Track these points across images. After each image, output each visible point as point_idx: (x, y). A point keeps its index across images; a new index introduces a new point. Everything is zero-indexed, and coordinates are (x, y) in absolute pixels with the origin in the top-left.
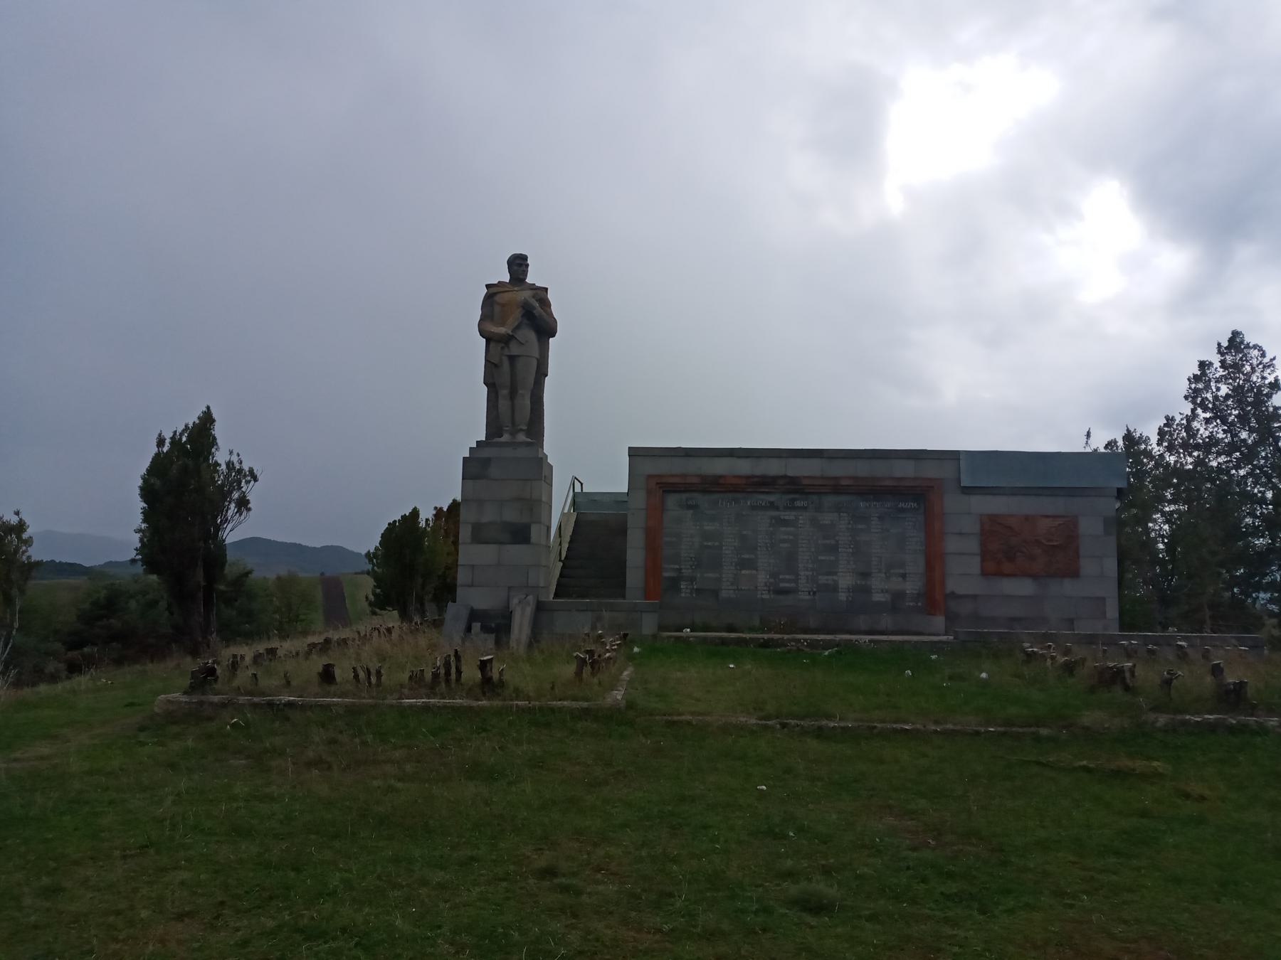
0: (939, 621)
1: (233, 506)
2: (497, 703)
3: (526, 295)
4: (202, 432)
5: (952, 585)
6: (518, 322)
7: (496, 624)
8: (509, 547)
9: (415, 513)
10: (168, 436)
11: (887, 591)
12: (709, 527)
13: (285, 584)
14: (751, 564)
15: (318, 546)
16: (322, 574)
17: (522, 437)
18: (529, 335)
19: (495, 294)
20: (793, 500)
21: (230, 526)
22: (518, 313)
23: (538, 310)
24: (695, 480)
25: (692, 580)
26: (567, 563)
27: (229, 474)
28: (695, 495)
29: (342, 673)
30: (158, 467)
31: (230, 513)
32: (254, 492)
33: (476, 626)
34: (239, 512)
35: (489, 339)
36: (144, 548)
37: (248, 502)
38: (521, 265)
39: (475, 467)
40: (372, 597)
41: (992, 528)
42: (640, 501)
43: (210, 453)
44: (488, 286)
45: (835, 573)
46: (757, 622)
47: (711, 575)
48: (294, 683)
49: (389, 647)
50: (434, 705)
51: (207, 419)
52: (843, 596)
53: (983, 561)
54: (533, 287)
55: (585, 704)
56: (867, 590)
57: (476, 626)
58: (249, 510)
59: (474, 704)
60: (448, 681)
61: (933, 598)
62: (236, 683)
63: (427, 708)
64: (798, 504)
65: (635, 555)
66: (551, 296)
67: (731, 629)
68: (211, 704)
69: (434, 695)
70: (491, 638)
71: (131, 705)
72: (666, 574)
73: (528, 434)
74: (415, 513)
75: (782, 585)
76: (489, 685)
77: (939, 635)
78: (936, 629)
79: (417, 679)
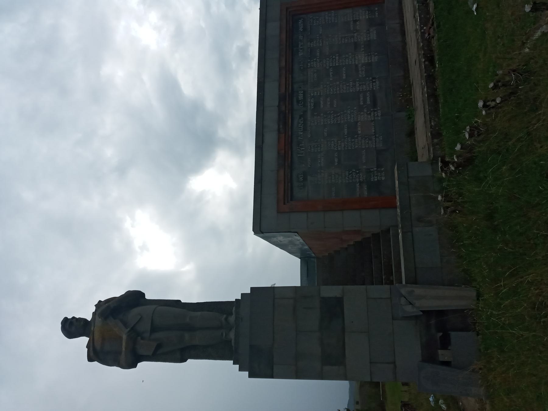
6: (130, 330)
17: (232, 319)
20: (298, 101)
24: (282, 173)
33: (443, 355)
45: (356, 66)
52: (375, 59)
65: (351, 220)
75: (368, 102)
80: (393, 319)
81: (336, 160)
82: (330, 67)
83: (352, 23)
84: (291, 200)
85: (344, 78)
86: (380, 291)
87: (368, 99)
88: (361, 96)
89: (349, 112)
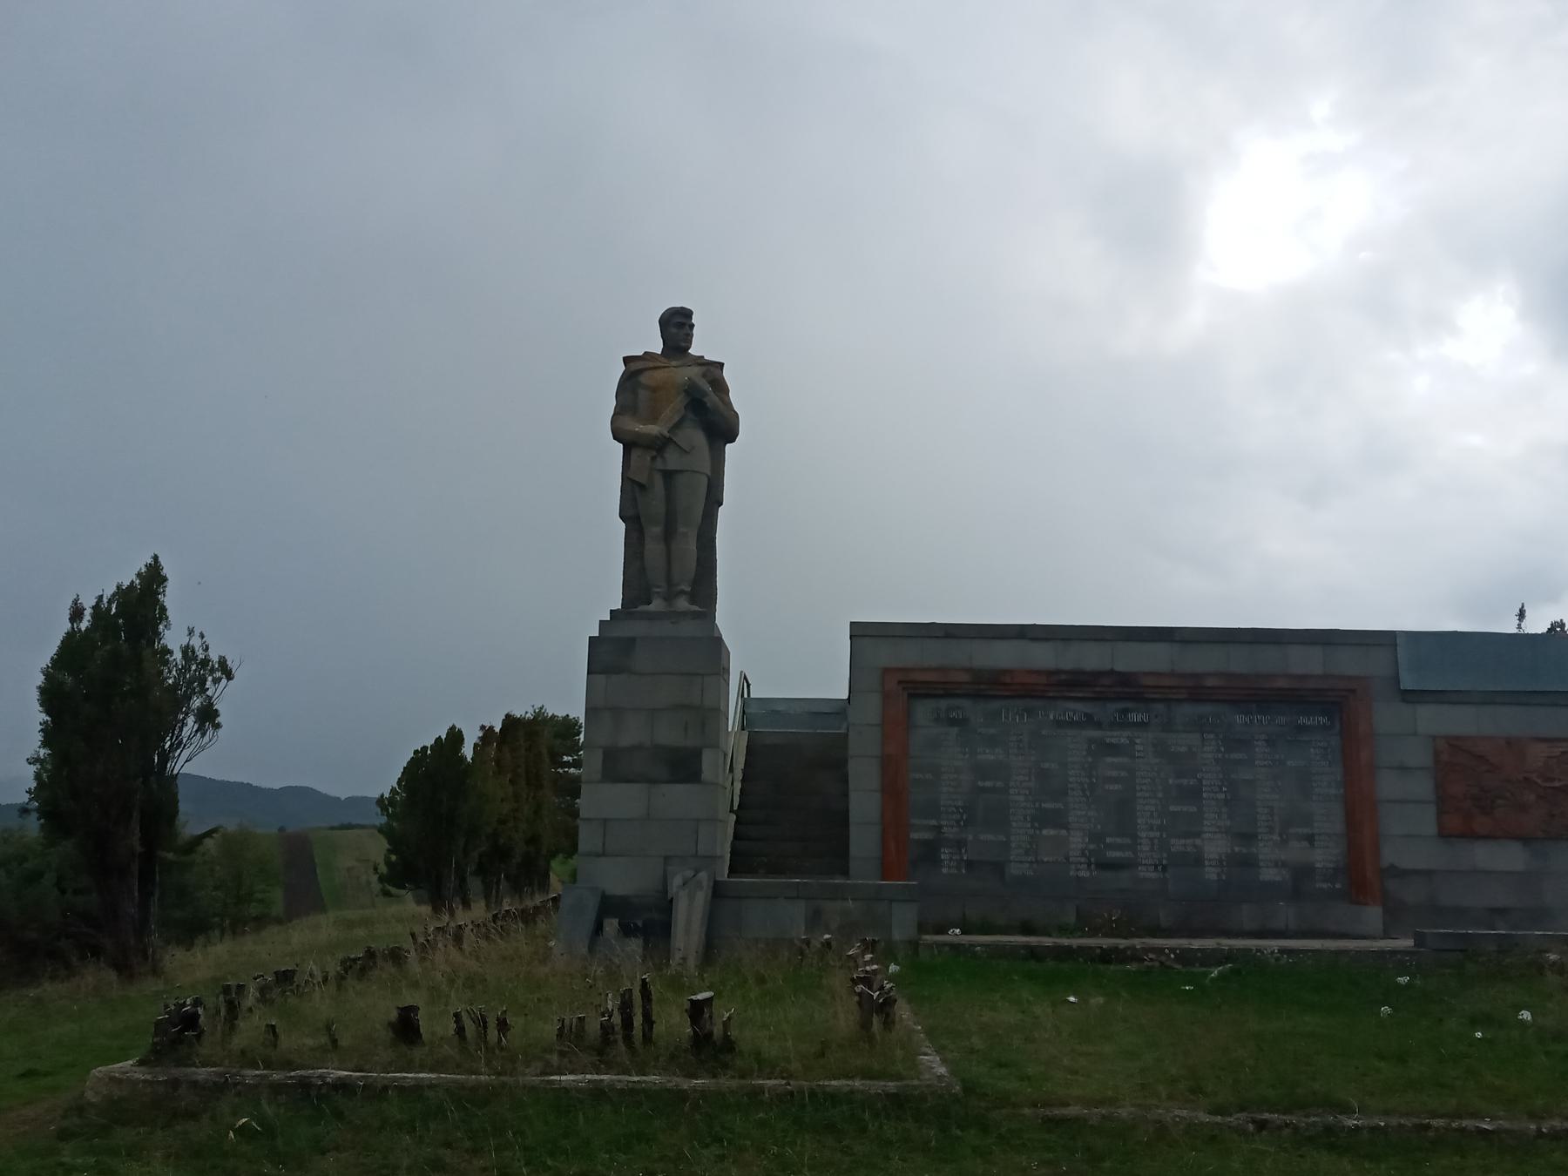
0: (1373, 915)
1: (191, 720)
2: (727, 1082)
3: (694, 372)
4: (140, 604)
5: (1392, 855)
6: (675, 418)
7: (647, 921)
8: (665, 788)
9: (455, 737)
10: (88, 603)
11: (1284, 864)
12: (988, 756)
13: (236, 845)
14: (1057, 820)
15: (277, 787)
16: (281, 829)
17: (683, 604)
18: (695, 437)
19: (640, 371)
20: (1125, 712)
21: (186, 754)
22: (679, 402)
23: (712, 399)
24: (965, 677)
25: (960, 844)
26: (743, 812)
27: (186, 668)
28: (966, 703)
29: (435, 1026)
30: (72, 653)
31: (186, 732)
32: (225, 697)
33: (611, 925)
34: (202, 730)
35: (630, 444)
36: (43, 788)
37: (216, 713)
38: (681, 325)
39: (608, 653)
40: (383, 869)
41: (1456, 763)
42: (871, 711)
43: (157, 634)
44: (627, 360)
45: (1198, 835)
46: (1071, 919)
47: (990, 837)
48: (344, 1042)
49: (458, 957)
50: (611, 1085)
51: (153, 577)
52: (1211, 873)
53: (1440, 813)
54: (700, 361)
55: (892, 1086)
56: (1249, 863)
57: (611, 925)
58: (218, 726)
59: (686, 1084)
60: (628, 1039)
61: (1359, 877)
62: (237, 1042)
63: (598, 1093)
64: (1134, 717)
65: (864, 804)
66: (727, 374)
67: (1027, 929)
68: (194, 1084)
69: (610, 1067)
70: (635, 945)
71: (29, 1074)
72: (914, 836)
73: (693, 599)
74: (455, 737)
76: (708, 1047)
77: (1373, 938)
78: (1370, 935)
79: (571, 1035)
80: (667, 859)
81: (988, 784)
82: (1200, 781)
83: (1306, 831)
84: (911, 696)
85: (1172, 808)
86: (723, 844)
87: (1118, 854)
88: (1127, 841)
89: (1091, 813)
